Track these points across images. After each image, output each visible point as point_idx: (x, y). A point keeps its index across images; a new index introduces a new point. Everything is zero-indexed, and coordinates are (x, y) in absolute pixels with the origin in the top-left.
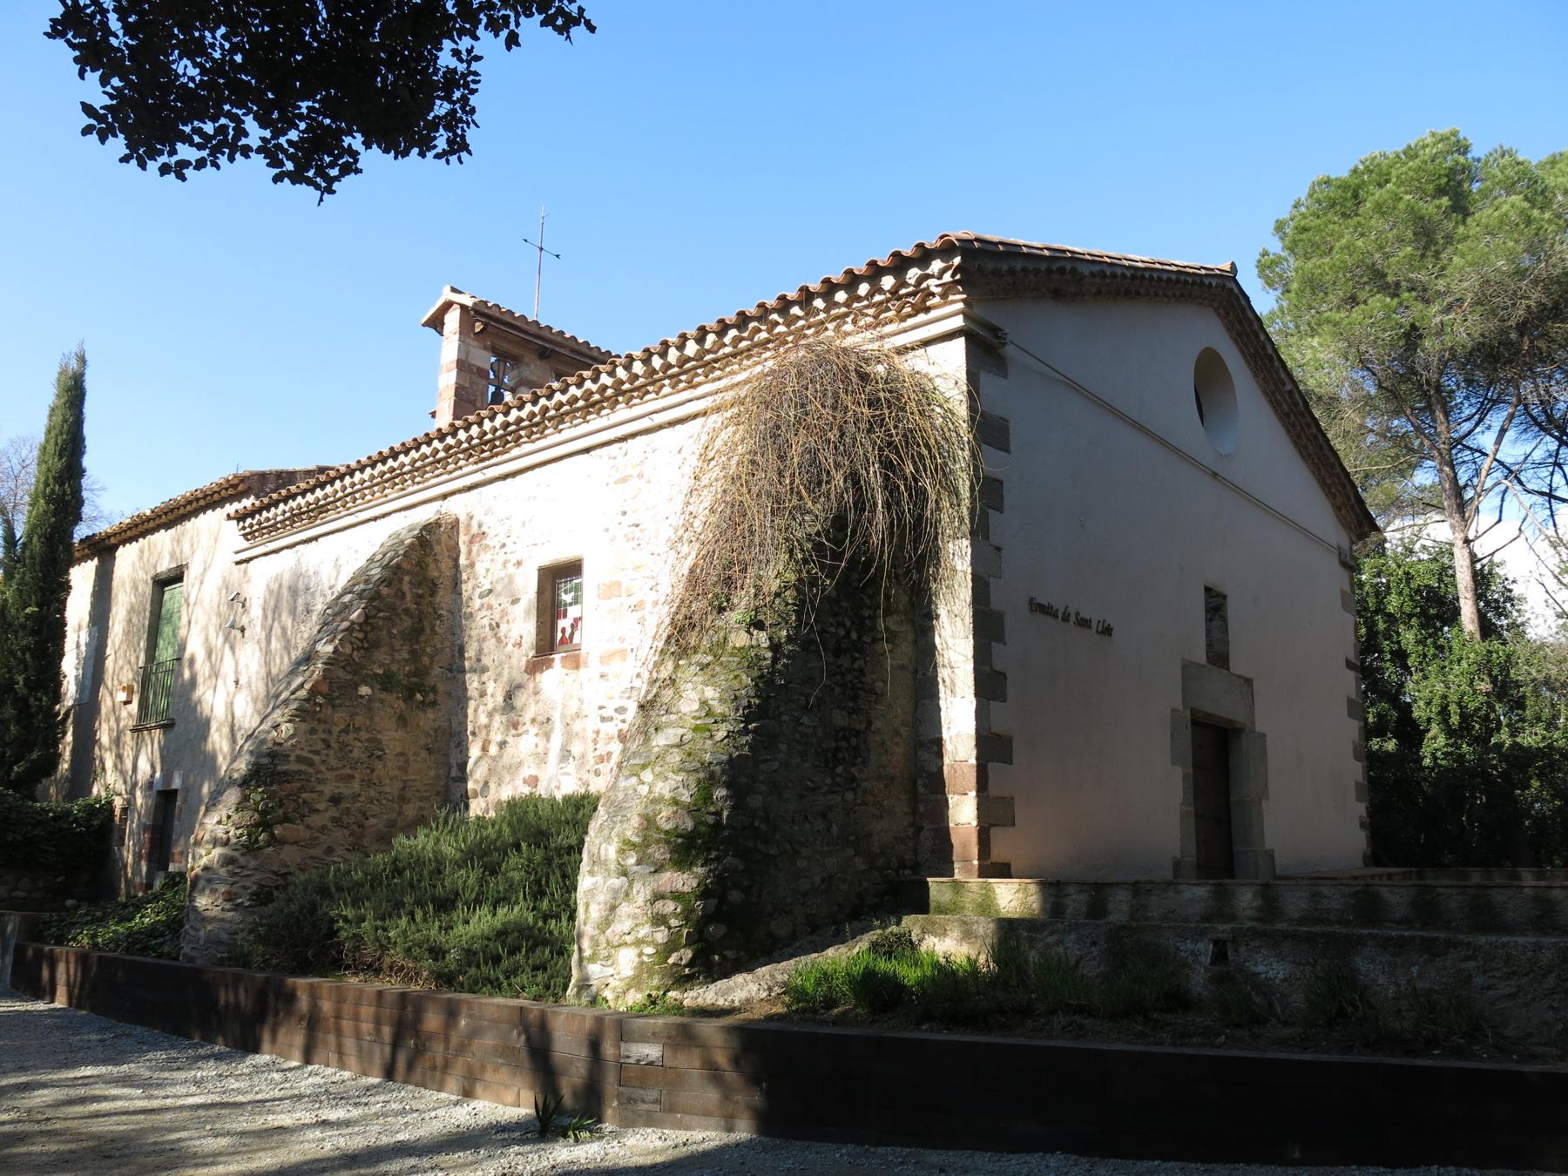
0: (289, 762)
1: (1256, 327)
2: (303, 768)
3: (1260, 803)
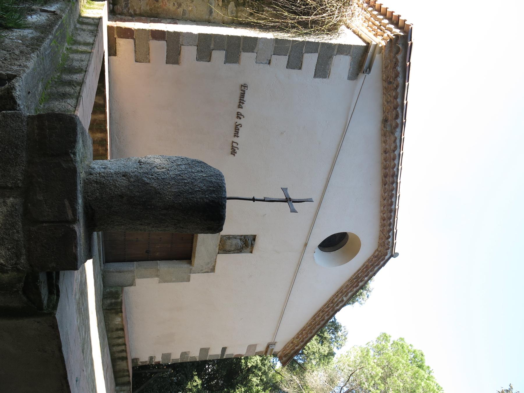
1: (371, 274)
3: (157, 276)
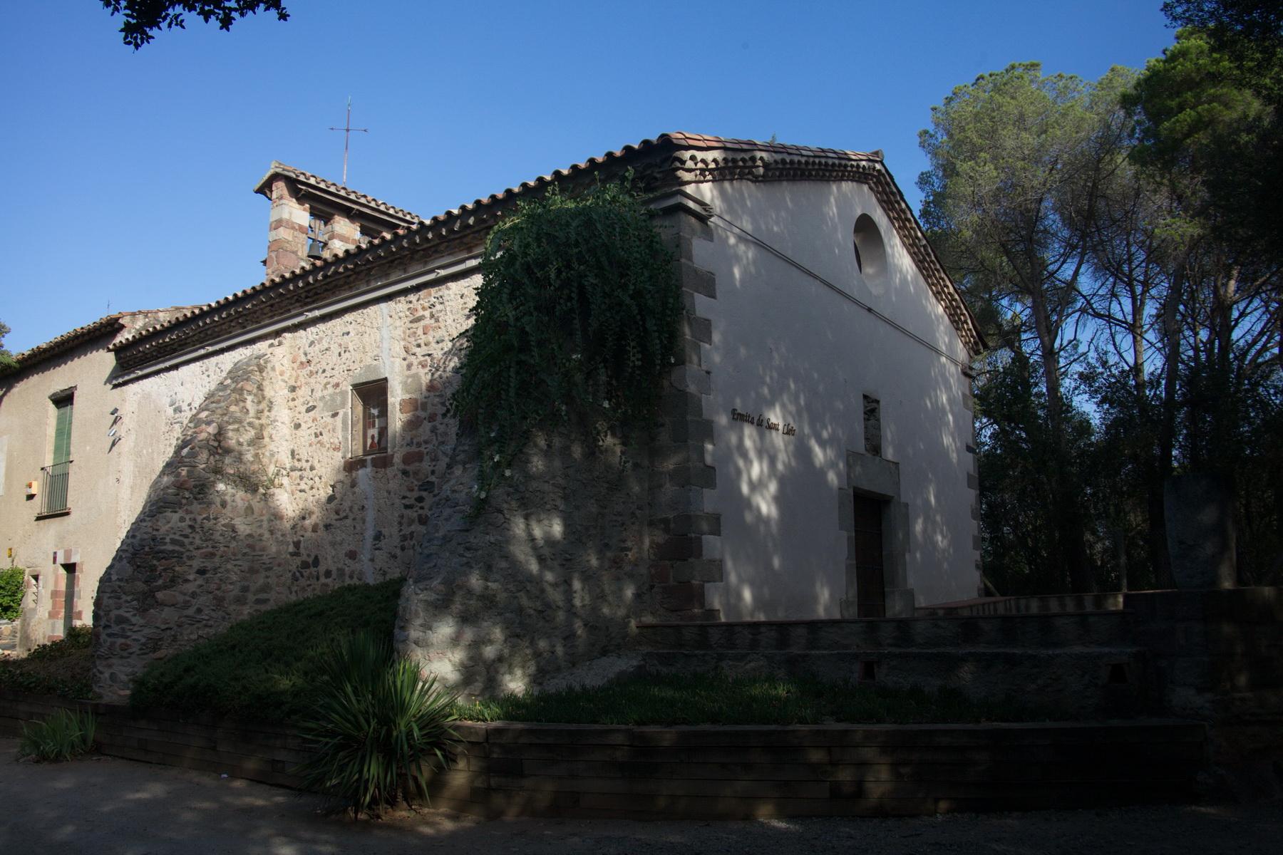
0: (165, 544)
2: (177, 548)
